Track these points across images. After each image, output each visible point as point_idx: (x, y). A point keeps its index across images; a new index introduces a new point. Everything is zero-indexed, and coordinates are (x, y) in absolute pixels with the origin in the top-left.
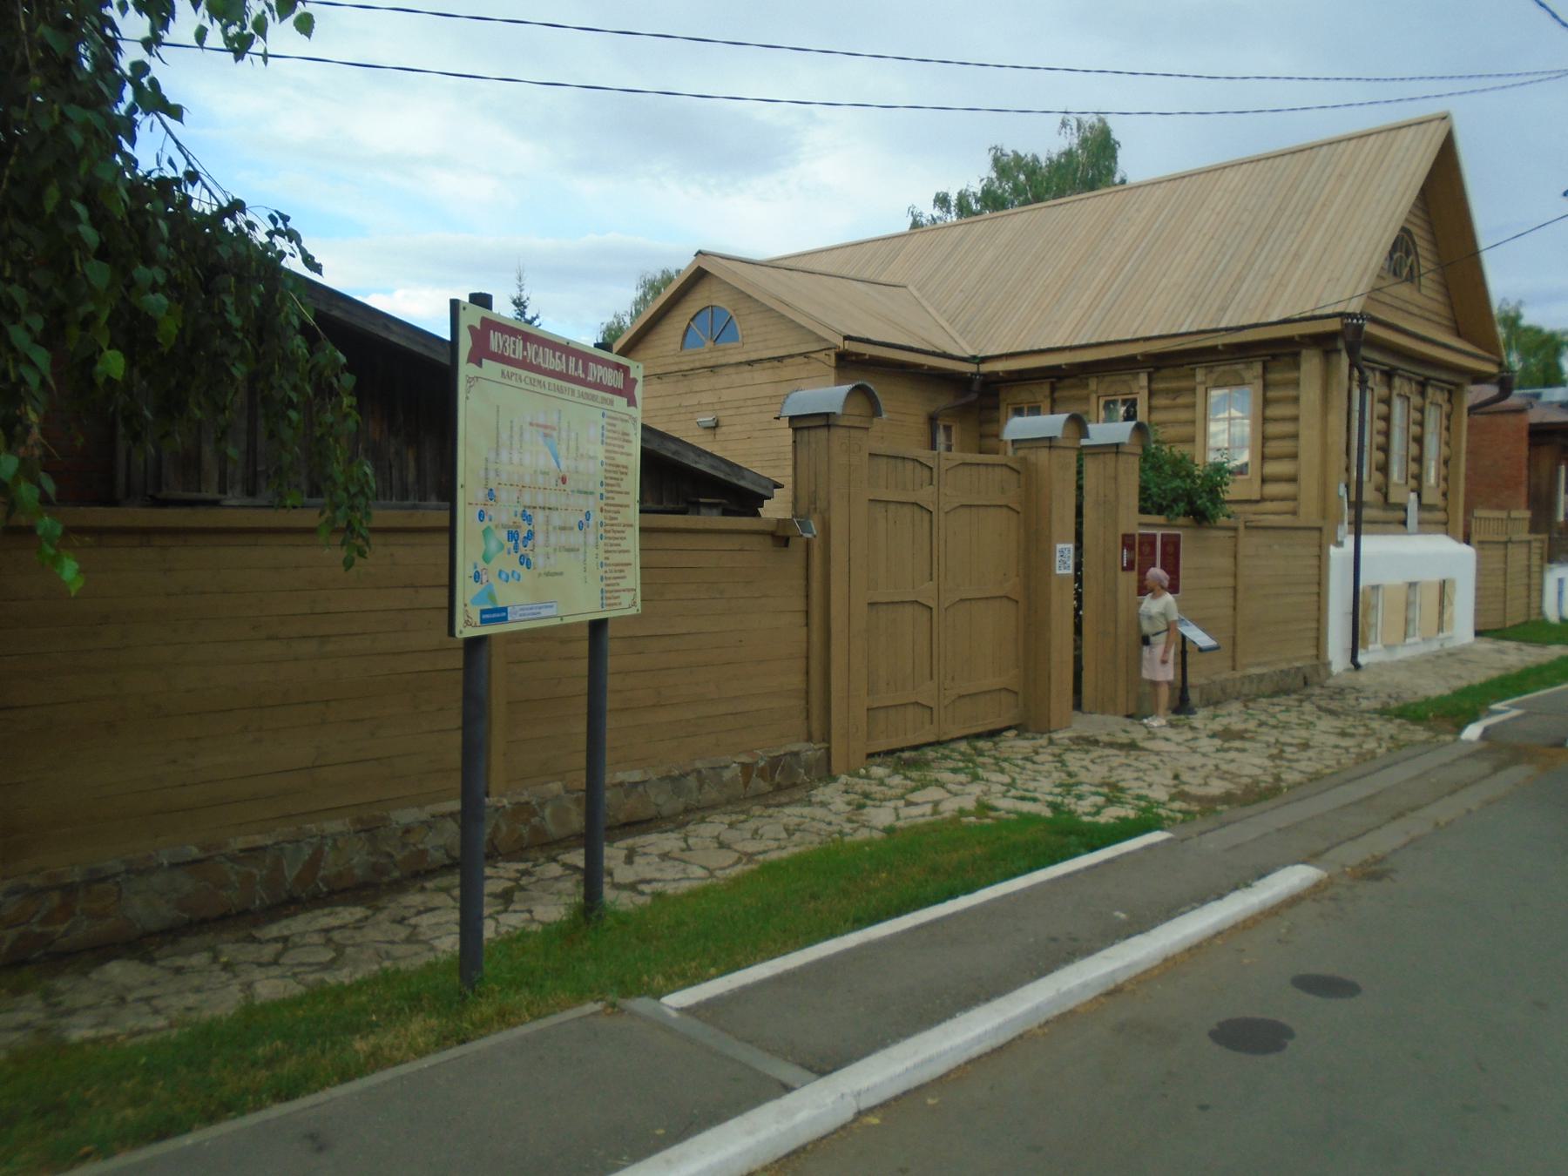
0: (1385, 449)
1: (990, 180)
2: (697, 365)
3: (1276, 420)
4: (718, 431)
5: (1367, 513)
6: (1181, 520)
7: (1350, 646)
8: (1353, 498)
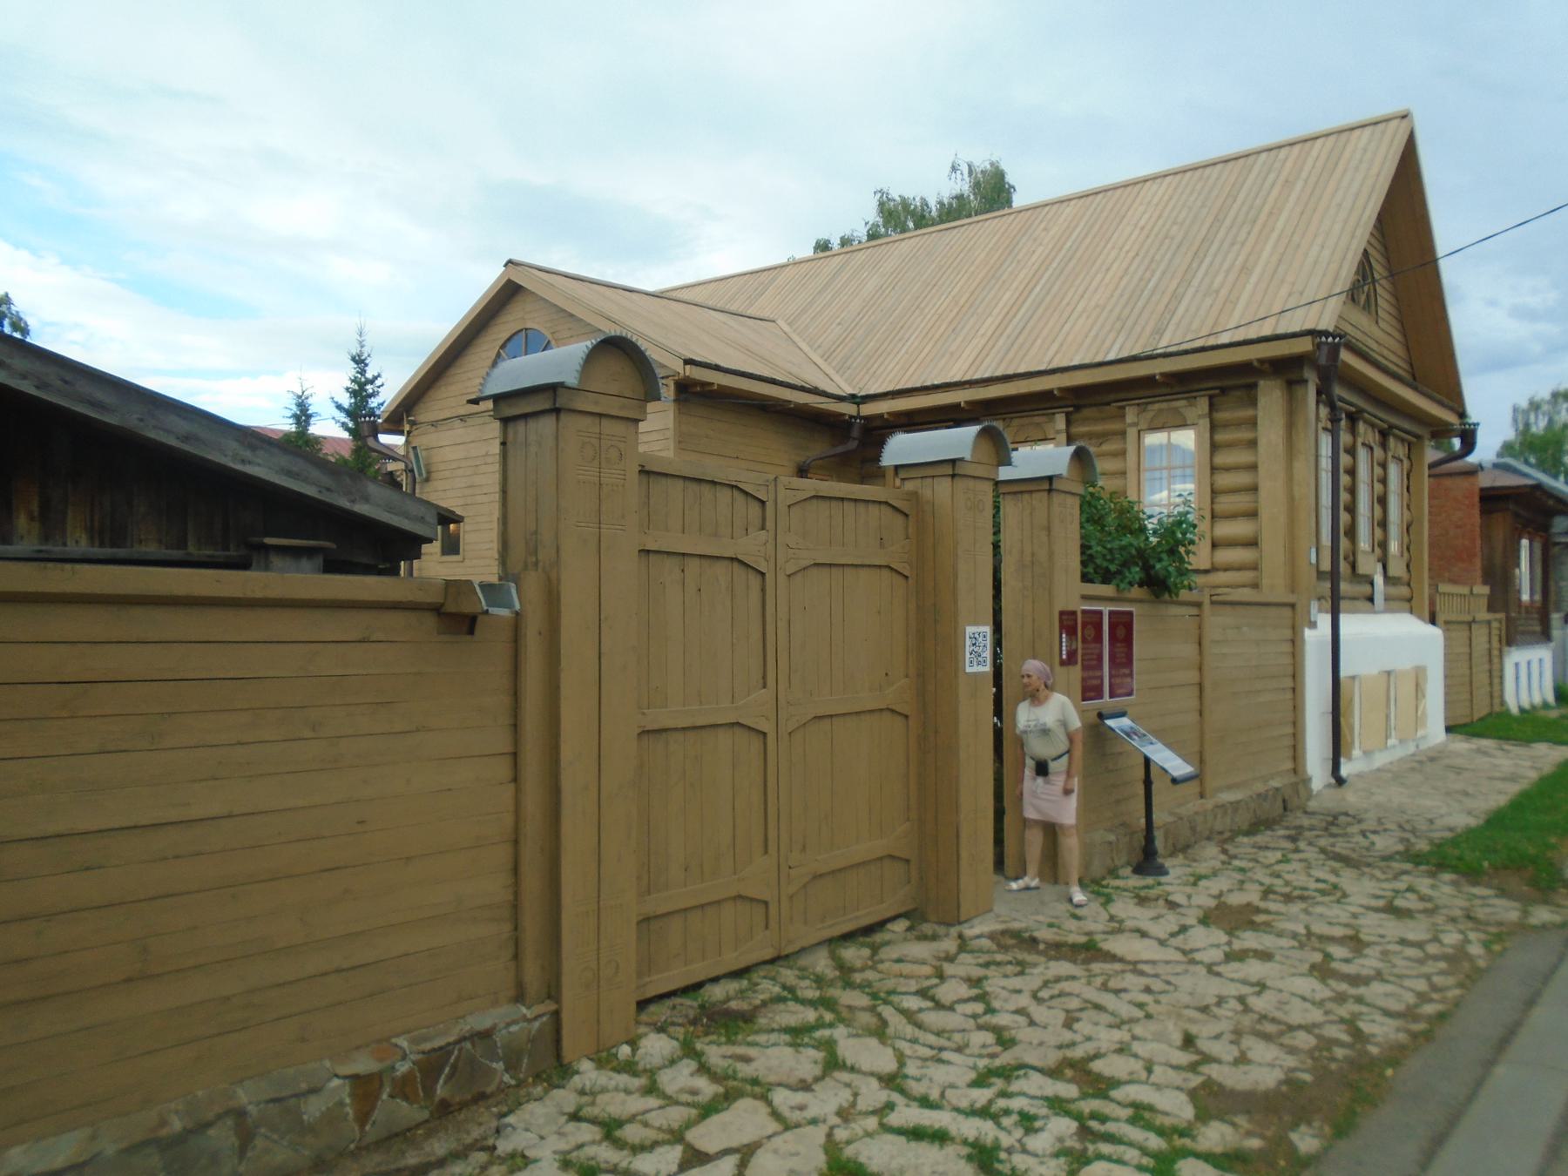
1: (876, 225)
3: (1228, 469)
6: (1136, 592)
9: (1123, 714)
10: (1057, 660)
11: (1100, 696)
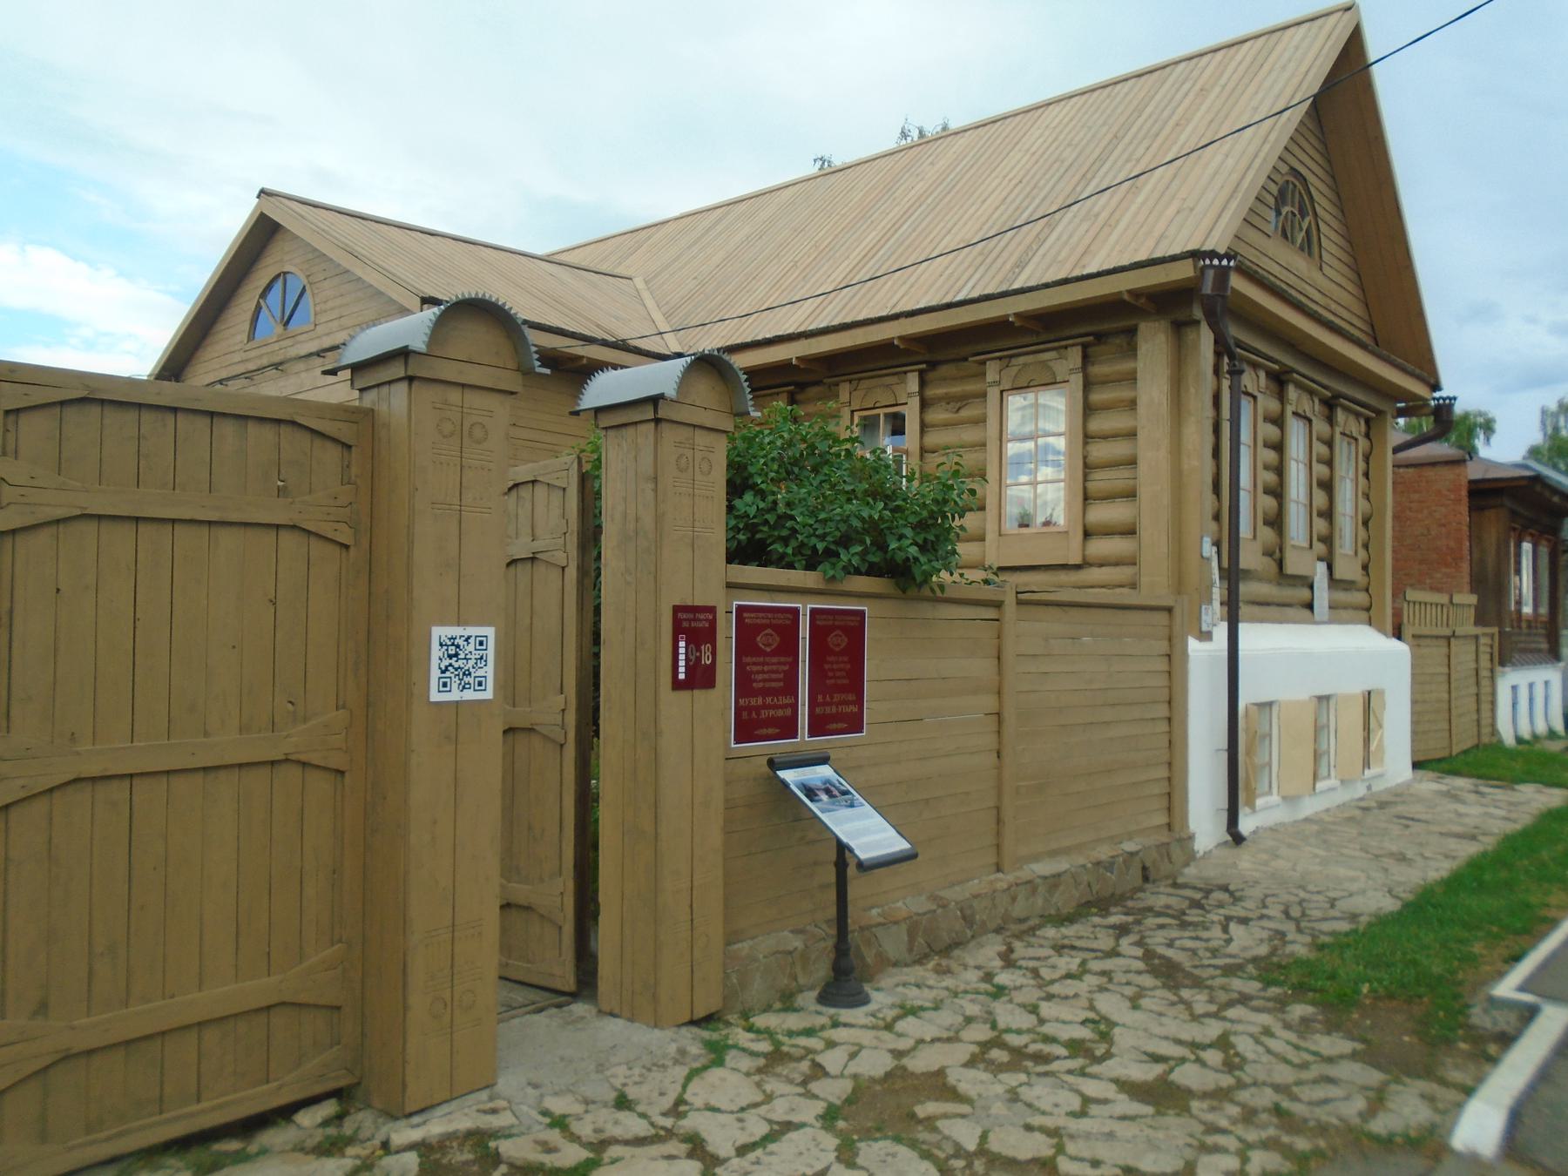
0: (1278, 492)
5: (1245, 589)
7: (1224, 803)
8: (1225, 564)
9: (824, 760)
10: (666, 679)
11: (793, 733)
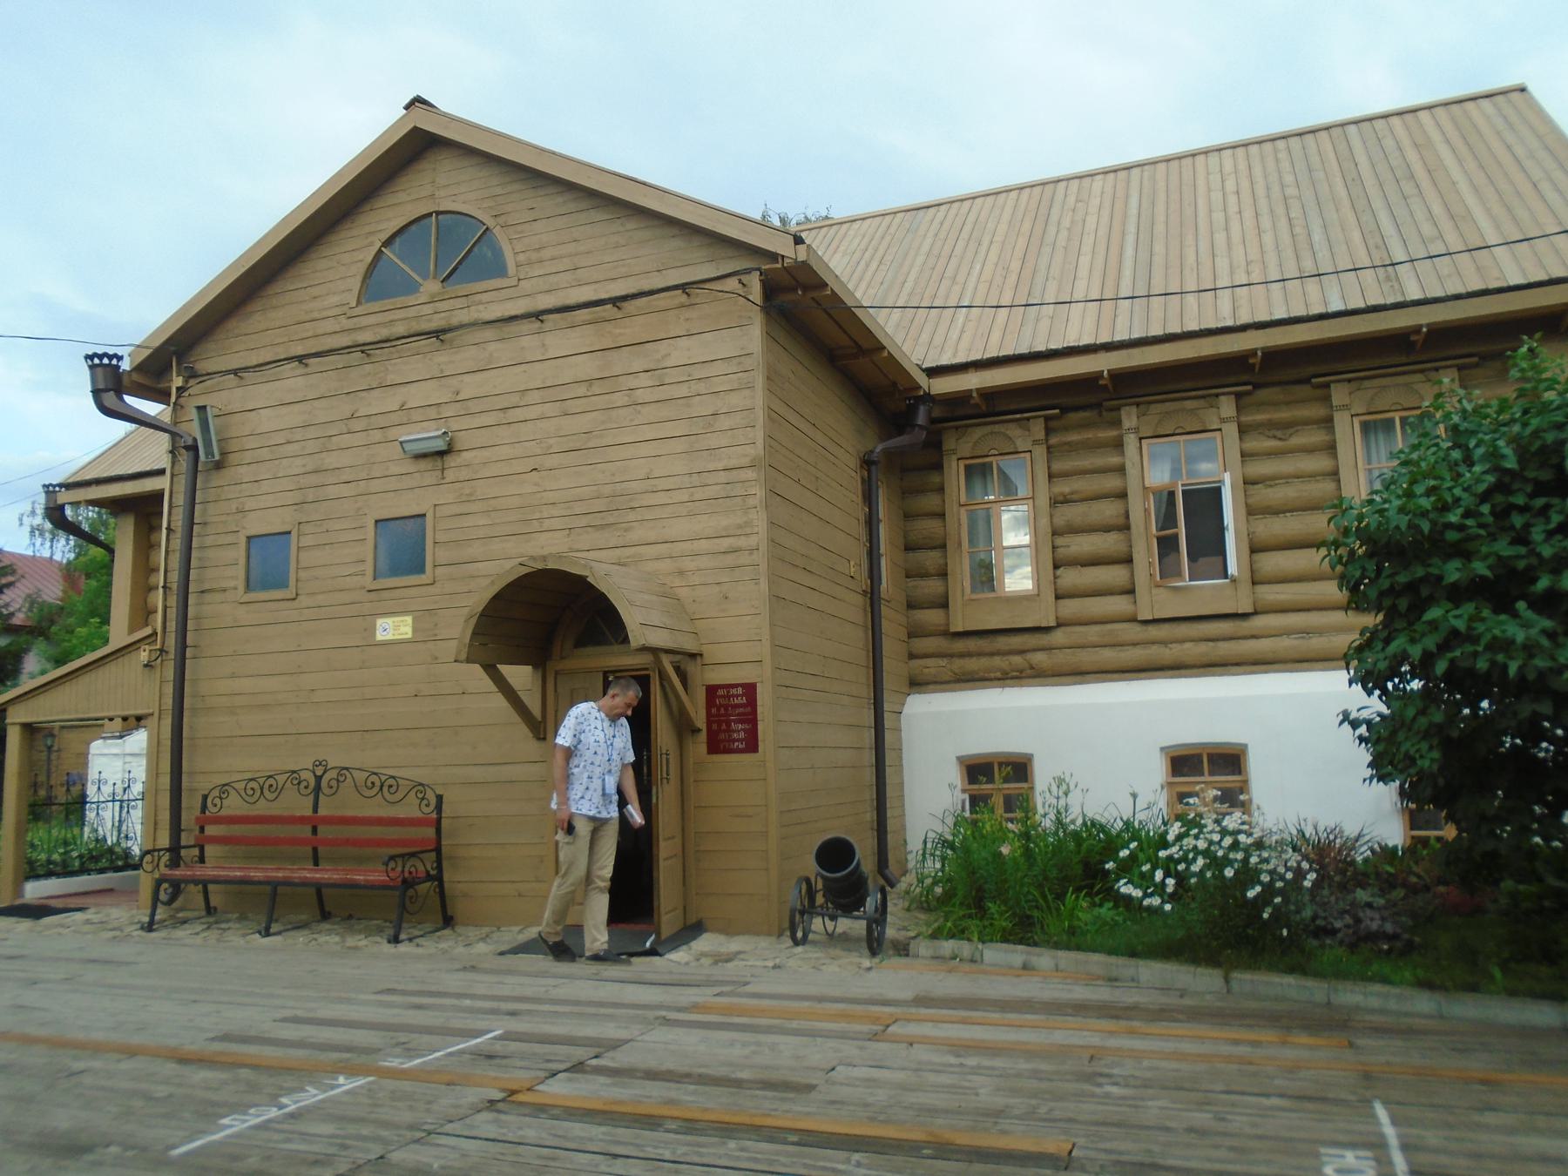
2: (400, 329)
4: (451, 461)
